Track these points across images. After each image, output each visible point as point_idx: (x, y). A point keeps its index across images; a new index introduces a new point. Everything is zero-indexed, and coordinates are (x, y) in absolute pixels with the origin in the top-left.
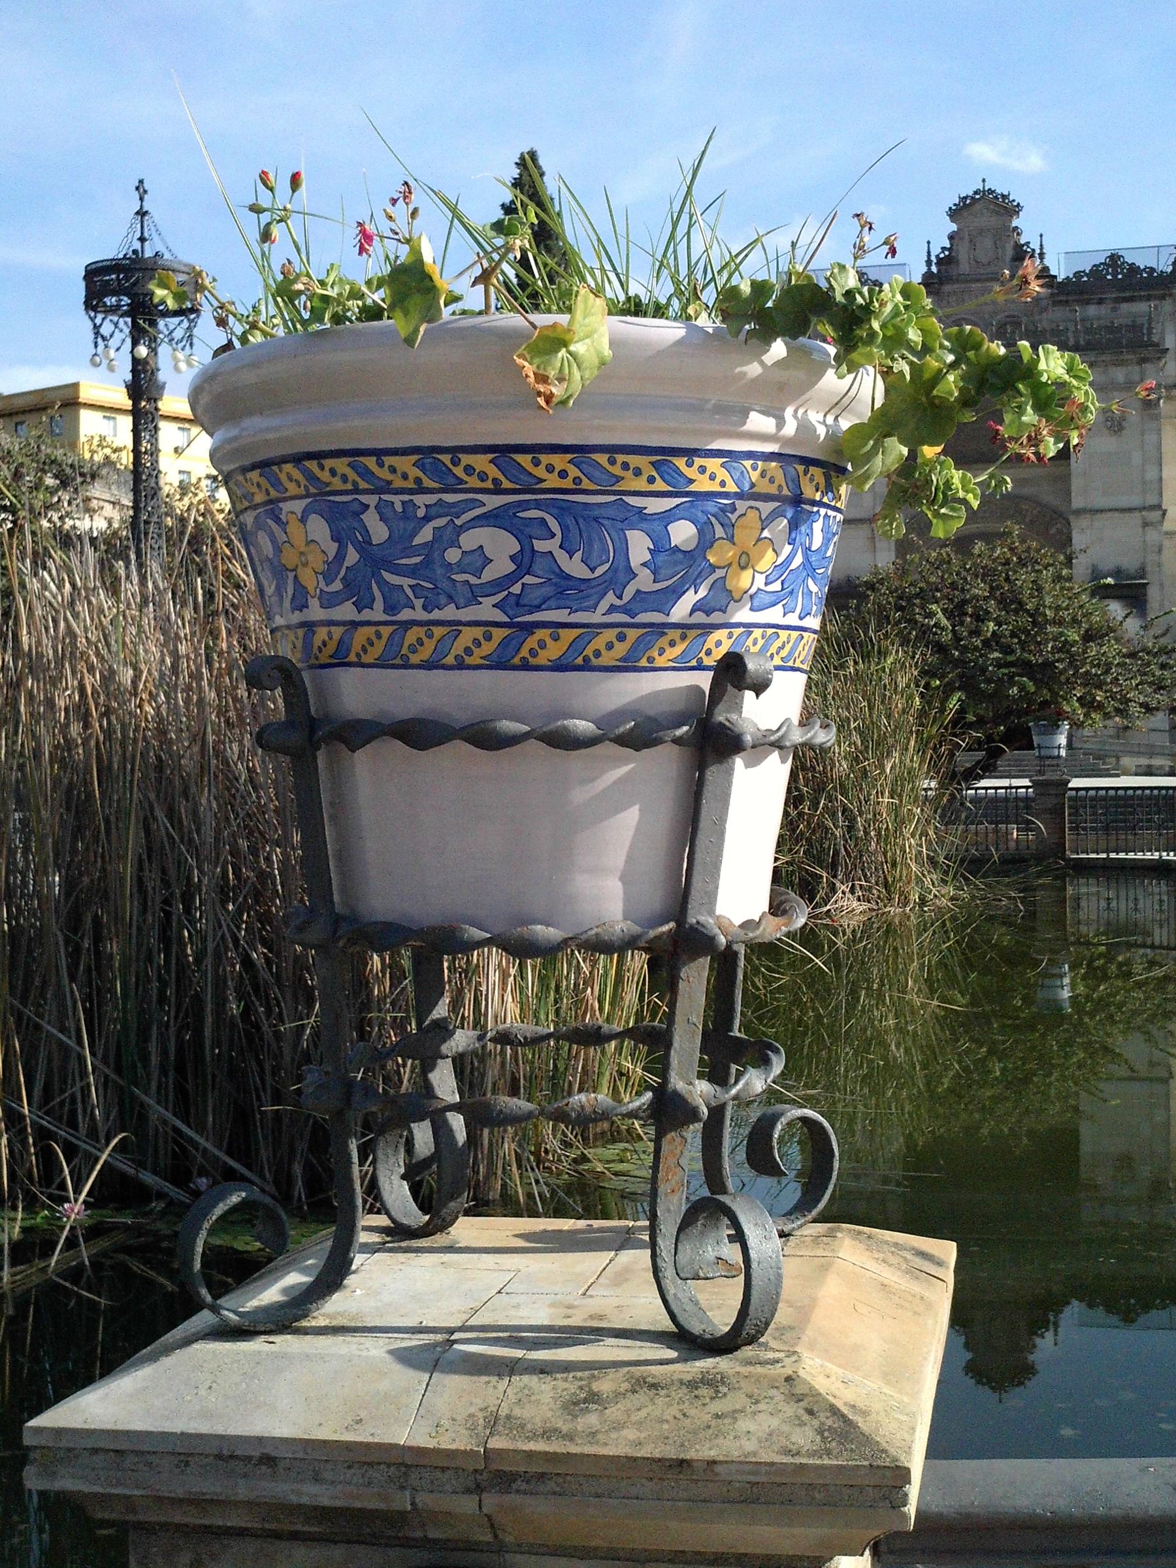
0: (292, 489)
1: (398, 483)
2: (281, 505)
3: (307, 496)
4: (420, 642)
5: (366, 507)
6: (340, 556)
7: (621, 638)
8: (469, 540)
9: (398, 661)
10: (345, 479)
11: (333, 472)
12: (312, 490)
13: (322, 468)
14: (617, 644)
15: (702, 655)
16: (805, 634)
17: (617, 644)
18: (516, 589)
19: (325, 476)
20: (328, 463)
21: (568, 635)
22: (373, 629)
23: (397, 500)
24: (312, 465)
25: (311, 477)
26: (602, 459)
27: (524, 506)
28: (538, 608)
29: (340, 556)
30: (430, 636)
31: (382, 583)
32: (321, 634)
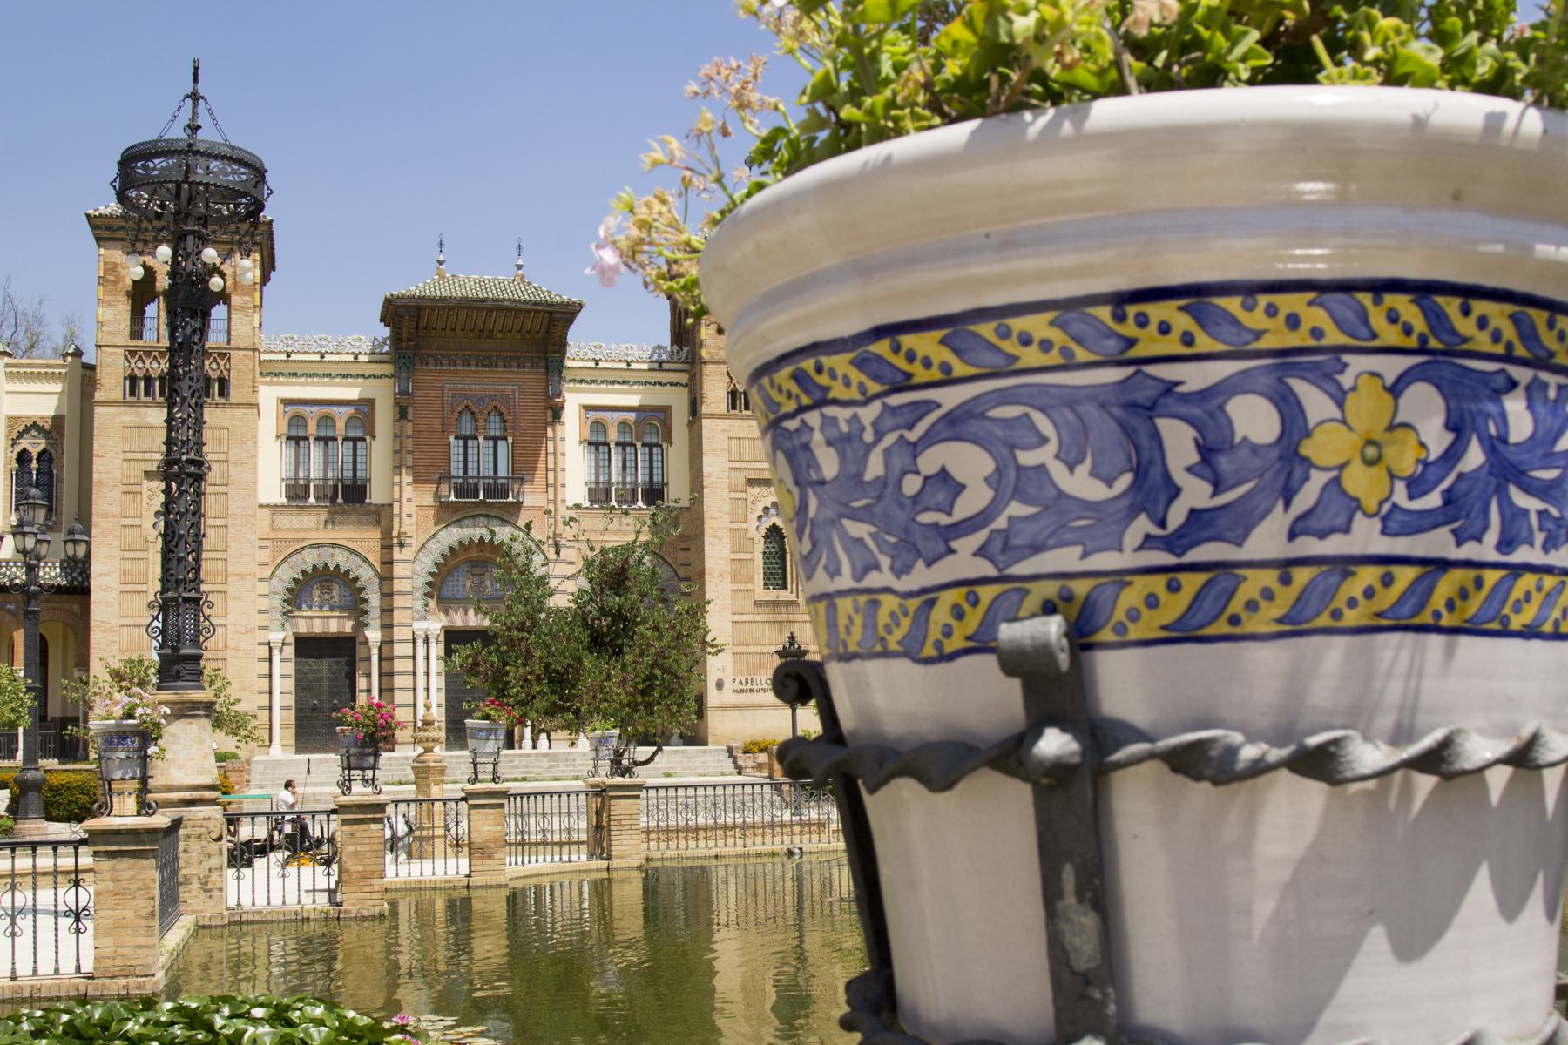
0: (1390, 335)
1: (921, 375)
2: (1346, 358)
3: (1421, 350)
4: (1464, 594)
5: (1513, 384)
6: (1452, 455)
7: (1387, 581)
8: (929, 462)
9: (1495, 626)
10: (1496, 337)
11: (1482, 323)
12: (1434, 344)
13: (1466, 312)
14: (1034, 348)
15: (1506, 611)
16: (1397, 570)
17: (1034, 348)
18: (1001, 523)
19: (1466, 326)
20: (1480, 307)
21: (1405, 576)
22: (1471, 574)
23: (843, 414)
24: (1451, 306)
25: (1436, 319)
26: (1232, 304)
27: (1005, 397)
28: (1037, 548)
29: (1452, 455)
30: (975, 602)
31: (1505, 502)
32: (889, 603)
